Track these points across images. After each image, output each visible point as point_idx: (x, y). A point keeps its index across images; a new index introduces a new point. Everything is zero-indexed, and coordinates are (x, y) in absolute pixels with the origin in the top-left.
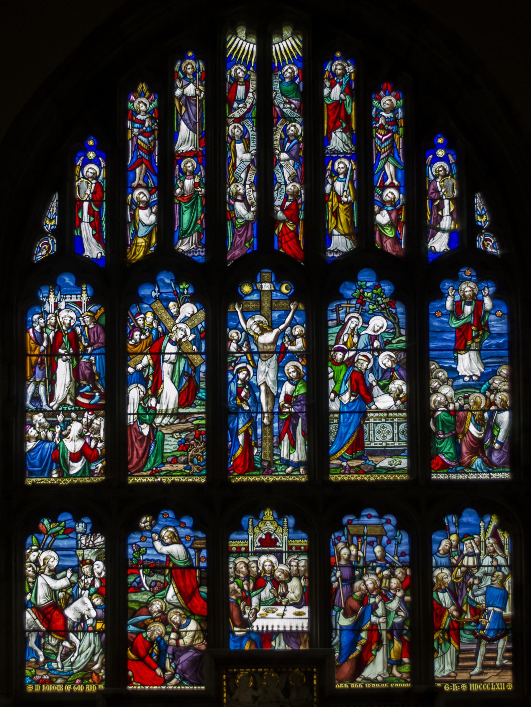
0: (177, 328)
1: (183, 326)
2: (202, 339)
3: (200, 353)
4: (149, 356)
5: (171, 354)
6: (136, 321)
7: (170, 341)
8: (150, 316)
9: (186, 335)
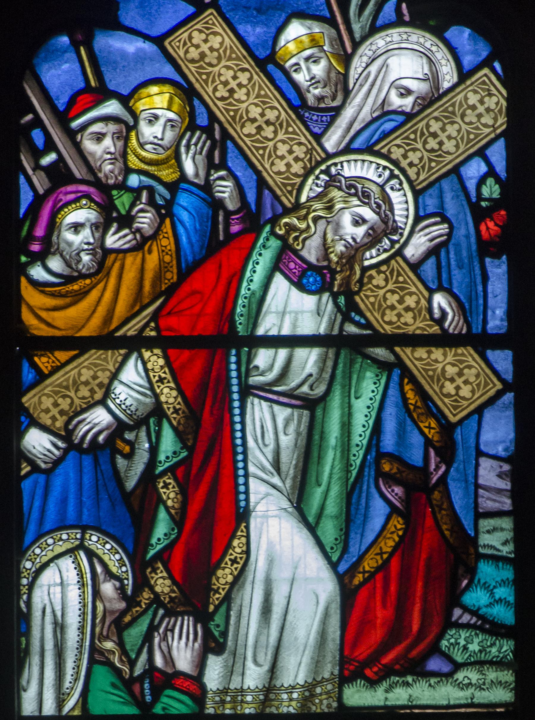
0: (333, 181)
1: (362, 169)
2: (486, 248)
3: (481, 342)
4: (156, 360)
5: (293, 341)
6: (72, 135)
7: (287, 260)
8: (157, 101)
9: (385, 229)
